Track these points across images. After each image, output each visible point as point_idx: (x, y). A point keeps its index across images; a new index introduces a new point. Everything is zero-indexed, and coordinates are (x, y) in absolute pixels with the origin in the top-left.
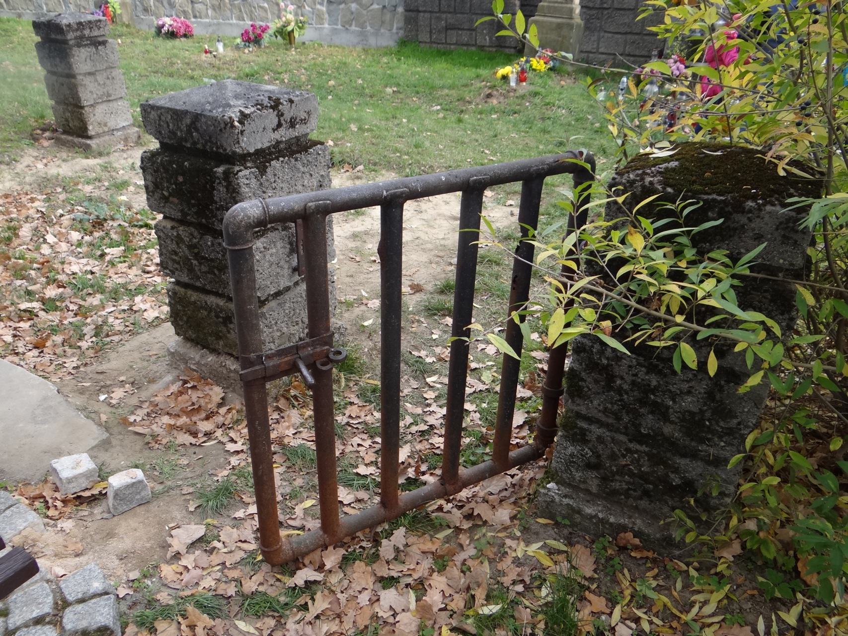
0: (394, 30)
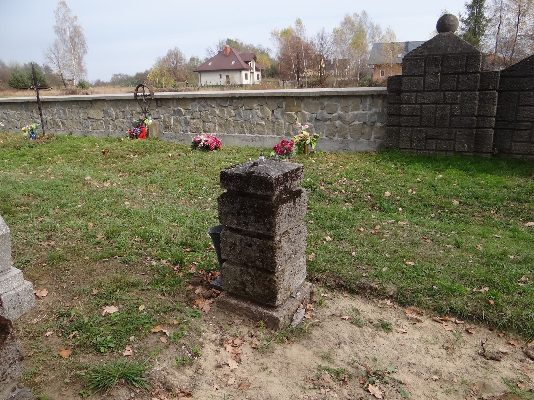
0: (372, 139)
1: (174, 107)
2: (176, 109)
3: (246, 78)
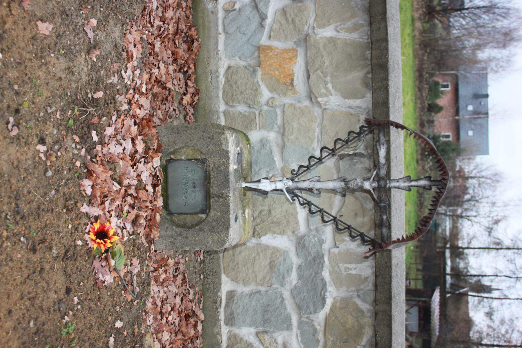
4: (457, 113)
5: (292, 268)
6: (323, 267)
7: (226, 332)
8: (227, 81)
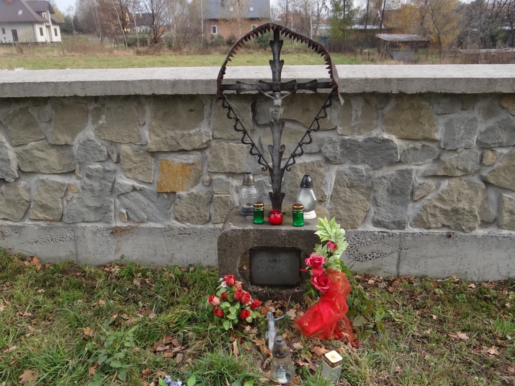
1: (353, 130)
2: (360, 138)
3: (42, 34)
4: (234, 20)
5: (353, 168)
6: (354, 141)
7: (411, 228)
8: (188, 220)
